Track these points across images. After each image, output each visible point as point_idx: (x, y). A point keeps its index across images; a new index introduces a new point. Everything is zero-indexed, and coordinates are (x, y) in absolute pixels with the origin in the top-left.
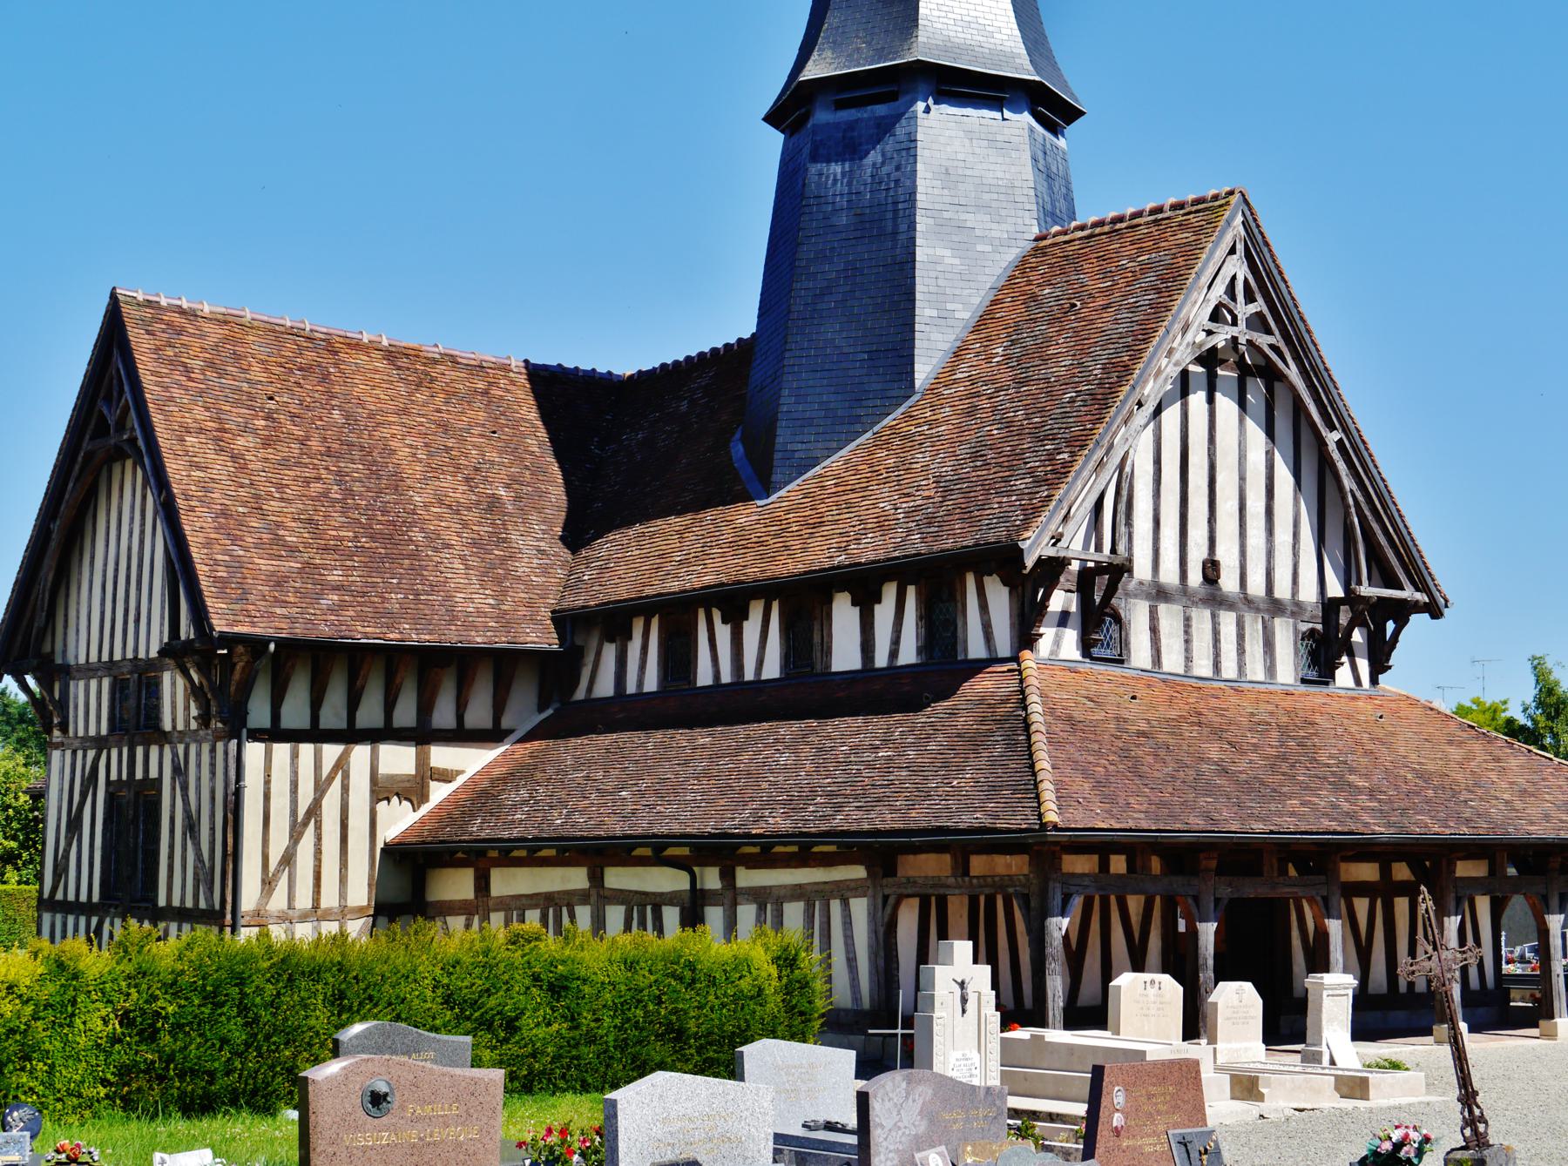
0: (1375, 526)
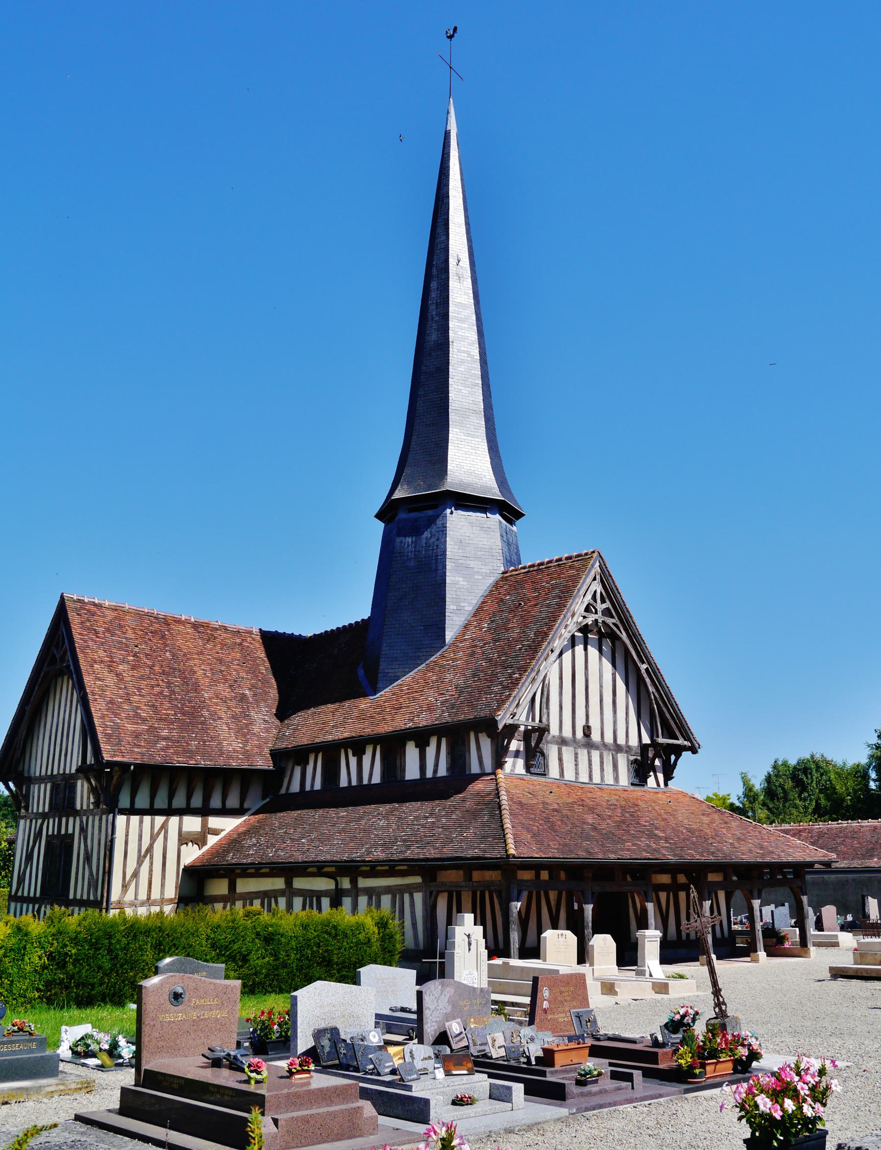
0: (664, 709)
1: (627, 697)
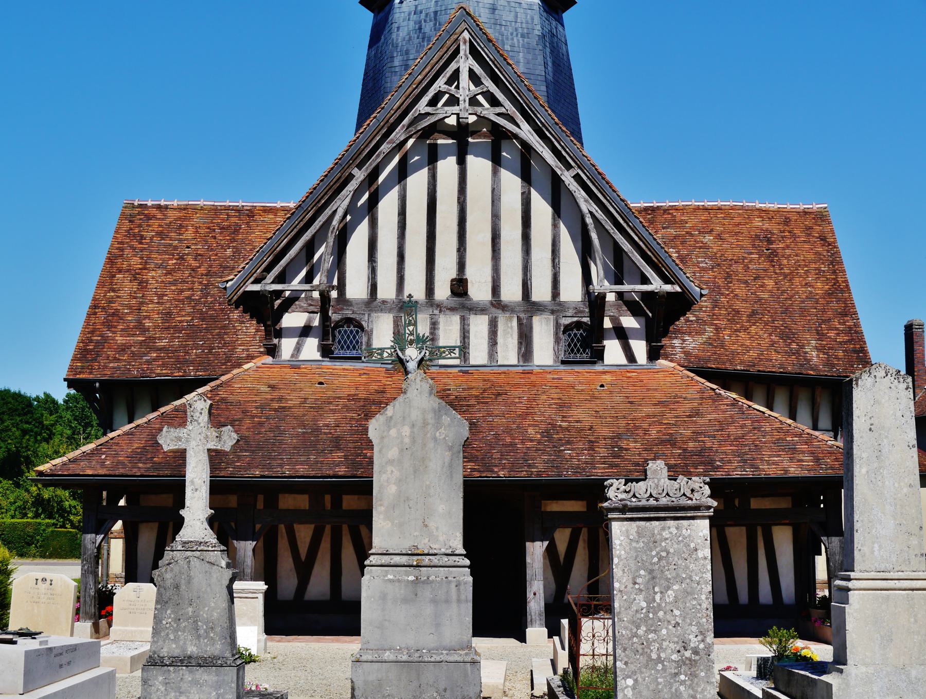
0: (619, 237)
1: (555, 226)
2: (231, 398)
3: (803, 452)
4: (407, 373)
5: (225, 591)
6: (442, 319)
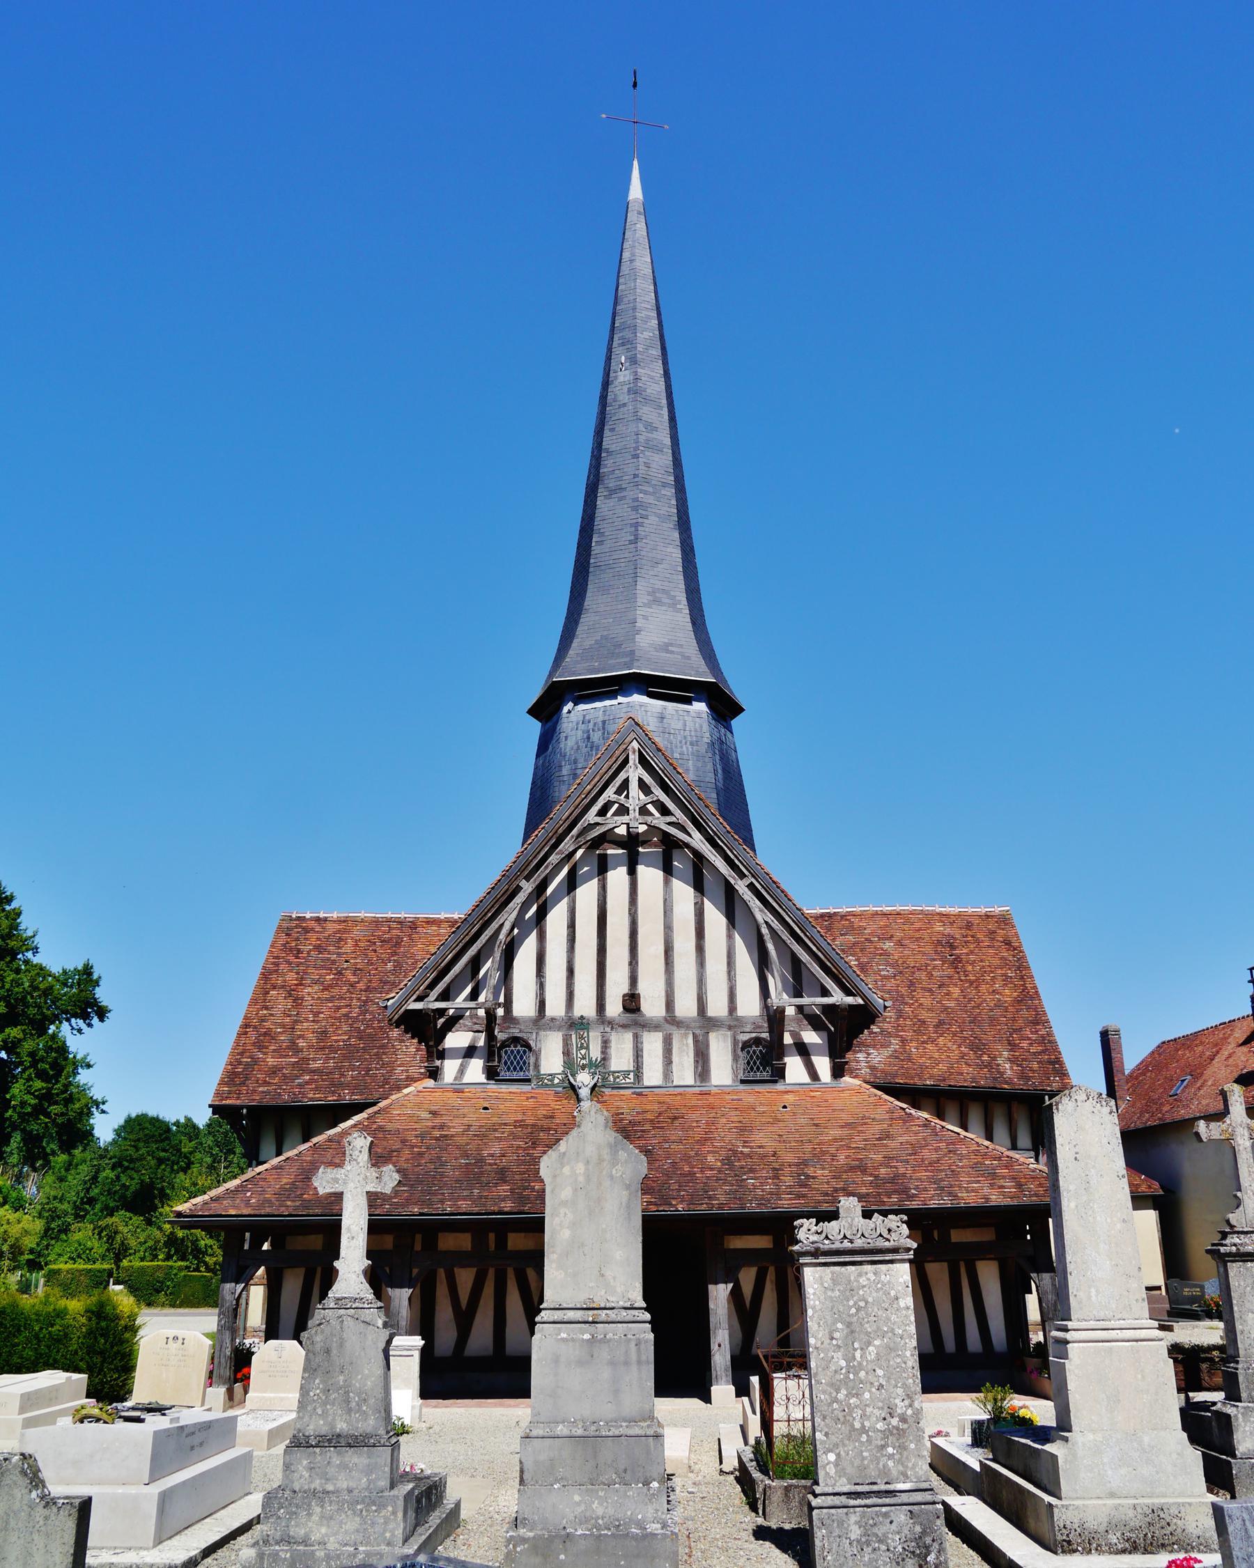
1: (730, 937)
2: (389, 1126)
3: (1004, 1177)
4: (579, 1100)
5: (381, 1356)
6: (614, 1037)
